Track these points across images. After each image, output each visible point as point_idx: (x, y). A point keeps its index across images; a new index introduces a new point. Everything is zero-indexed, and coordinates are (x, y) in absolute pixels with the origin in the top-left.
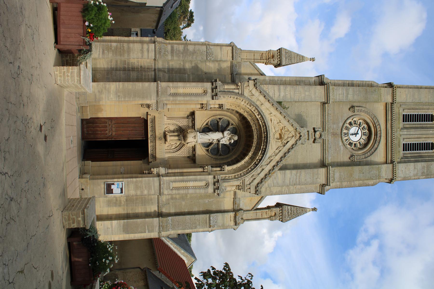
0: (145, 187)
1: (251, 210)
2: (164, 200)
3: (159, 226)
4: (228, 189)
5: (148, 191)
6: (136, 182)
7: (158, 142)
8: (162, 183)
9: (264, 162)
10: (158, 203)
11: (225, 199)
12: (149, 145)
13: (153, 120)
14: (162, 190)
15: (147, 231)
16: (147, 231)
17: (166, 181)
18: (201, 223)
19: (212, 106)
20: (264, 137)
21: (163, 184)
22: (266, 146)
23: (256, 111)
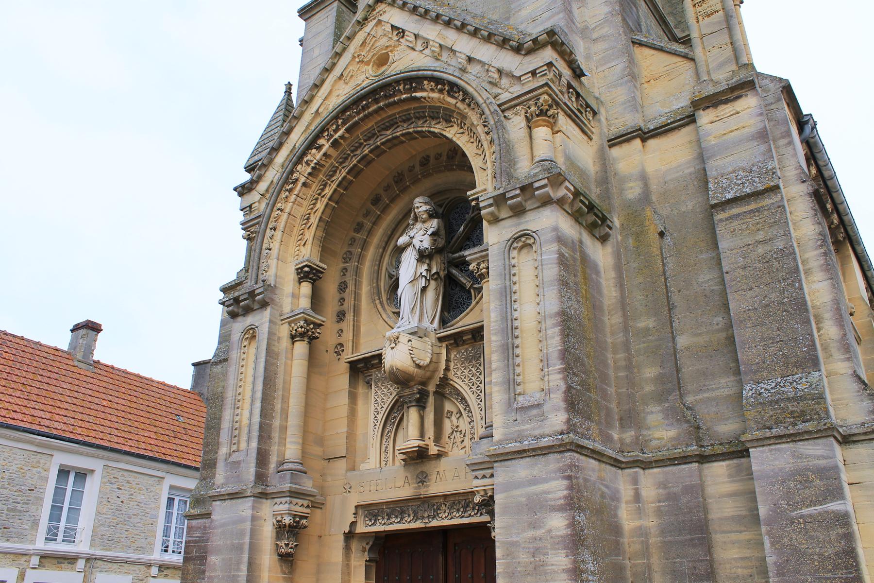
0: (534, 526)
1: (693, 60)
2: (672, 433)
3: (794, 438)
4: (542, 151)
5: (554, 509)
7: (436, 488)
8: (513, 446)
9: (448, 69)
10: (685, 459)
11: (650, 169)
12: (447, 522)
13: (371, 511)
14: (545, 442)
15: (834, 506)
16: (834, 506)
17: (506, 425)
19: (305, 303)
20: (377, 101)
21: (520, 439)
22: (397, 82)
23: (308, 157)
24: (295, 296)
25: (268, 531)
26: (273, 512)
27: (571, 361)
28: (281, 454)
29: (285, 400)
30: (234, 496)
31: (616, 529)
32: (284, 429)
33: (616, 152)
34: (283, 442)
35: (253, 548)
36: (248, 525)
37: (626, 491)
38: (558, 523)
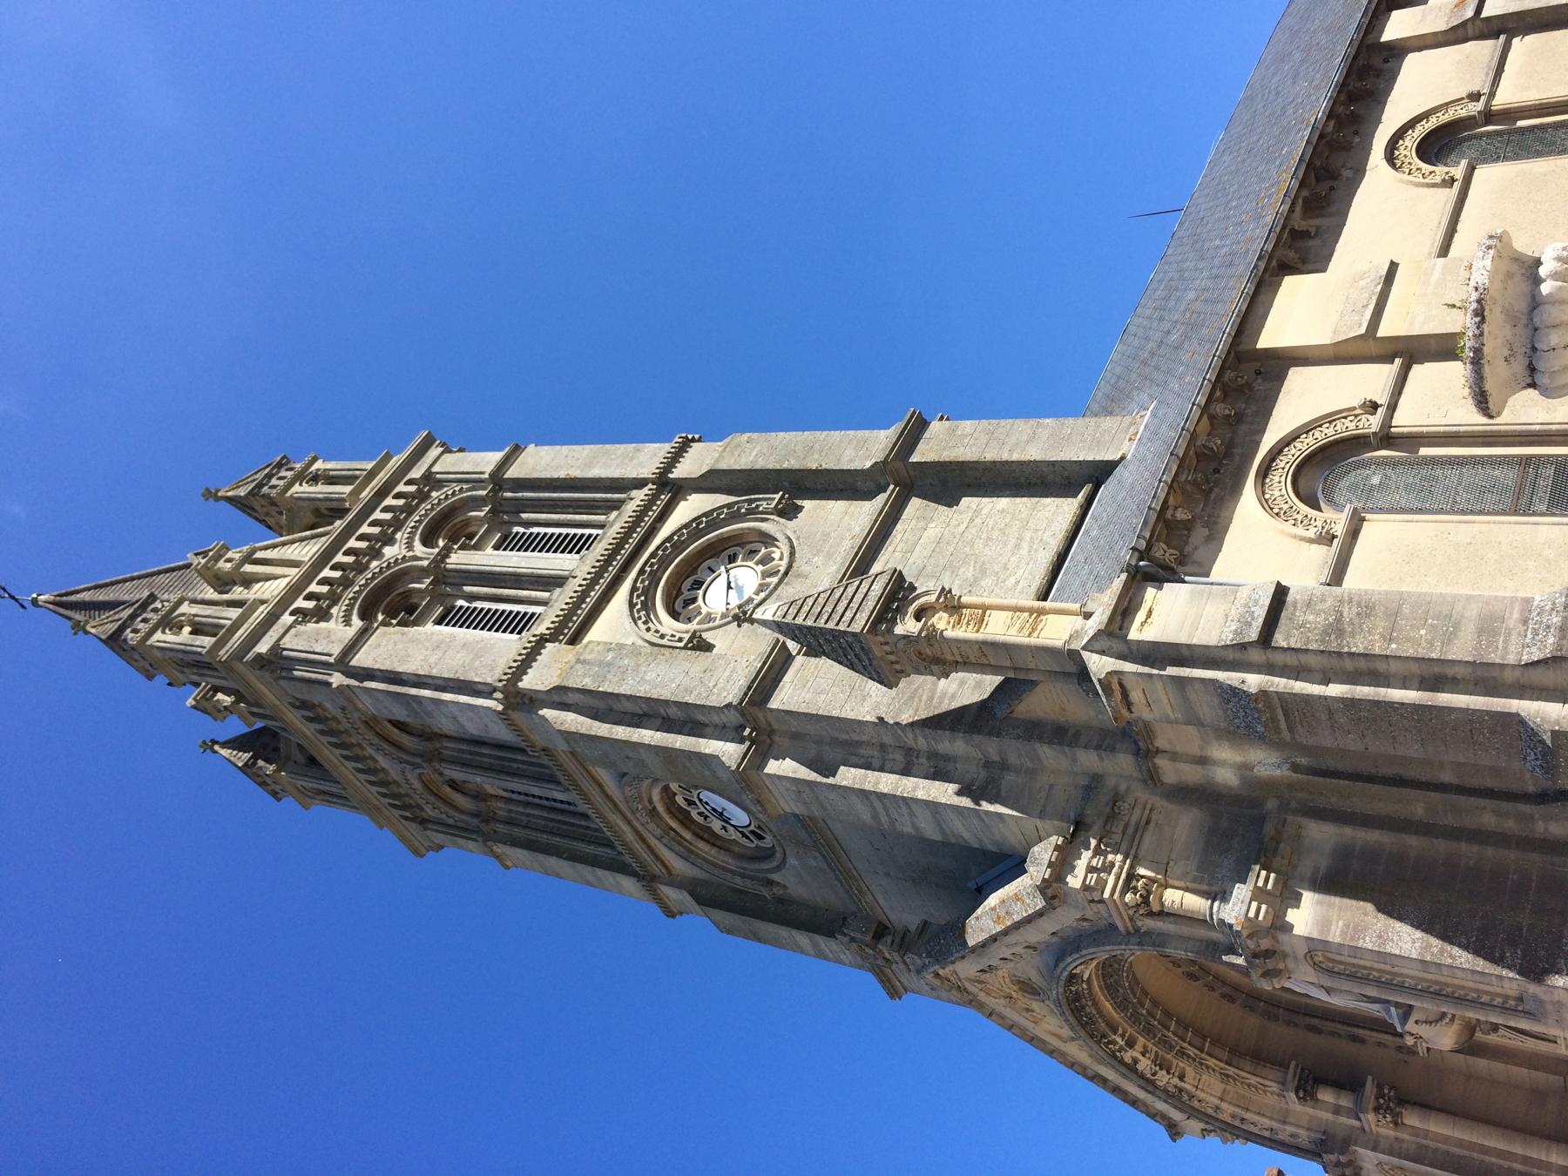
29: (1486, 1150)
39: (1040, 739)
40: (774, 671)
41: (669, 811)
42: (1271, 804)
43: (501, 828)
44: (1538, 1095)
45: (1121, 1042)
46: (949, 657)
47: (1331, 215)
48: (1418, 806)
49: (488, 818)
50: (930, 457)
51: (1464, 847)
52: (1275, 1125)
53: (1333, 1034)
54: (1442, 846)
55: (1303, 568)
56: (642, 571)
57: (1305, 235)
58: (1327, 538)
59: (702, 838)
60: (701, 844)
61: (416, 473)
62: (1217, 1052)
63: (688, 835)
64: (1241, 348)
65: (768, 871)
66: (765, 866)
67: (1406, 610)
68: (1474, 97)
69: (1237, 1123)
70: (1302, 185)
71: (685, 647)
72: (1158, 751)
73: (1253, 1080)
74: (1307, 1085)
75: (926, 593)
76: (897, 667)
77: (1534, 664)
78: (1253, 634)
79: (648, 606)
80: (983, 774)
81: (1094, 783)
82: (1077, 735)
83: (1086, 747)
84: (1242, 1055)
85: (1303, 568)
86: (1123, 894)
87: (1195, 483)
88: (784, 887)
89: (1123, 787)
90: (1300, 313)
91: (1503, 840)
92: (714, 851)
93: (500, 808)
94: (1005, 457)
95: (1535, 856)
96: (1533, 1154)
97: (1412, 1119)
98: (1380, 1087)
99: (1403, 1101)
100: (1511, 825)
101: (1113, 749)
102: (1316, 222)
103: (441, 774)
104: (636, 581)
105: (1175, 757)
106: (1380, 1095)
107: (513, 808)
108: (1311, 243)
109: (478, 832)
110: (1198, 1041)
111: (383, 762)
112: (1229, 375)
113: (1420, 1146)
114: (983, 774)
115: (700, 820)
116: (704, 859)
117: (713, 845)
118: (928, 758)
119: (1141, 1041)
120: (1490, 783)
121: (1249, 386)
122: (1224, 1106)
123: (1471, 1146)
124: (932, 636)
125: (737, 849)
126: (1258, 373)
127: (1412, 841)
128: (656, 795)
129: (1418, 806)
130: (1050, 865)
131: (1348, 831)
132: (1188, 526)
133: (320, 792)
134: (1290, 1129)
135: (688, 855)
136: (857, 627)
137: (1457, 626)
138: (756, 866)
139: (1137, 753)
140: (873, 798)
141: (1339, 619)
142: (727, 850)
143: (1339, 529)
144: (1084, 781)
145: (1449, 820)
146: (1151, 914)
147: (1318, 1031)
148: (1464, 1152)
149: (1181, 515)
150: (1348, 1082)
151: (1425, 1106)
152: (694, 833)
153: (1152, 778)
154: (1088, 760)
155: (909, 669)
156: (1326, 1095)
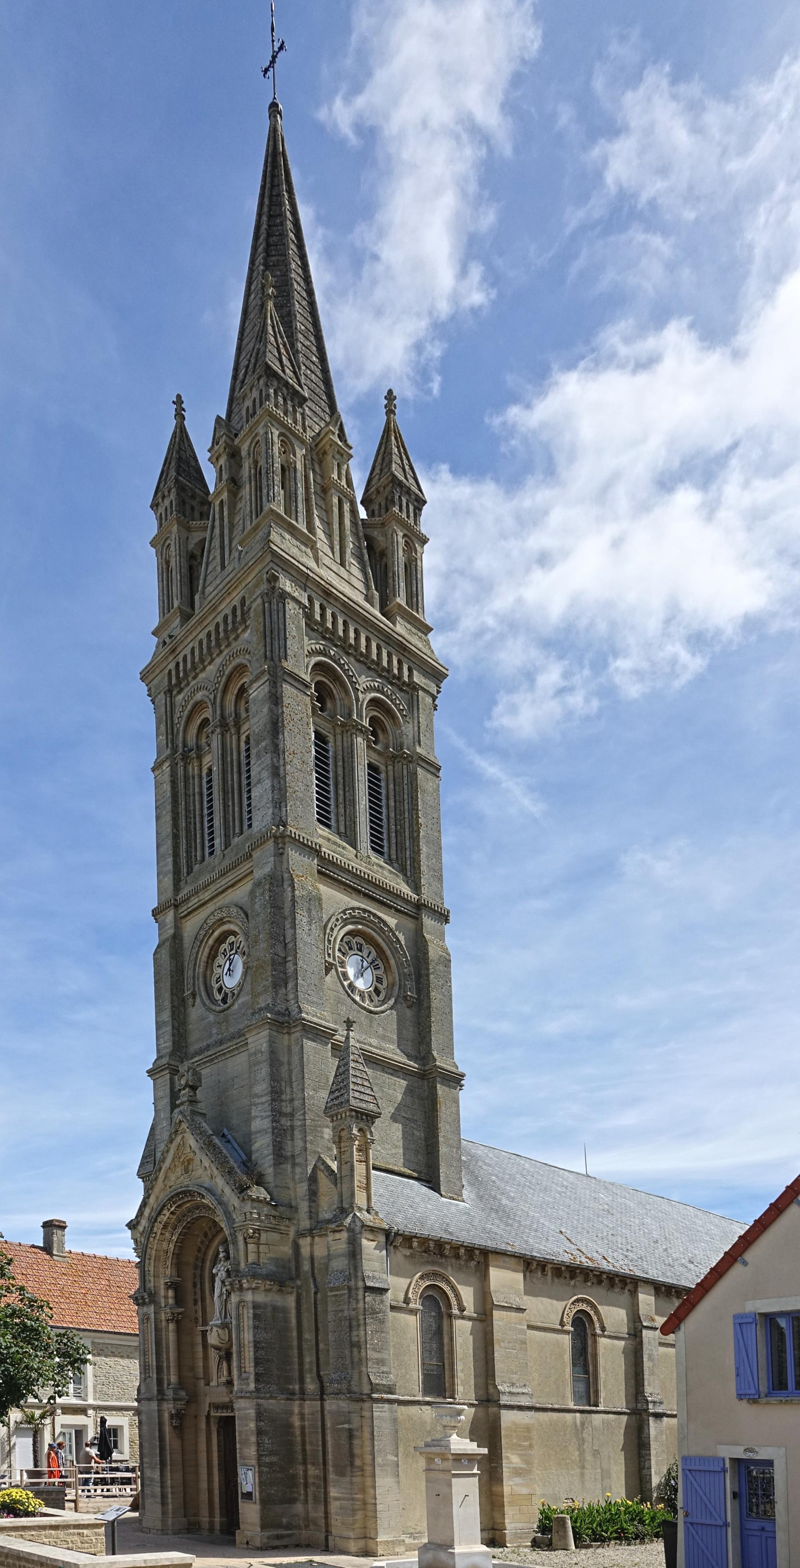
5: (251, 1420)
6: (240, 1443)
18: (340, 1308)
24: (166, 1297)
25: (166, 1416)
26: (169, 1407)
27: (257, 1362)
28: (169, 1380)
29: (168, 1353)
30: (149, 1399)
31: (290, 1426)
32: (168, 1367)
33: (305, 1242)
34: (169, 1374)
35: (161, 1424)
36: (156, 1414)
37: (296, 1410)
38: (252, 1425)
39: (310, 1185)
40: (320, 1034)
41: (224, 932)
42: (299, 1283)
43: (180, 771)
44: (193, 1369)
45: (172, 1209)
46: (342, 1145)
47: (552, 1280)
48: (308, 1336)
49: (185, 758)
50: (440, 1092)
51: (296, 1351)
52: (152, 1273)
53: (195, 1293)
54: (295, 1343)
55: (394, 1296)
56: (365, 911)
57: (543, 1270)
58: (407, 1301)
59: (211, 950)
60: (207, 950)
61: (418, 678)
62: (177, 1248)
63: (211, 942)
64: (490, 1256)
65: (201, 996)
66: (203, 994)
67: (383, 1335)
68: (603, 1329)
69: (147, 1257)
70: (567, 1267)
71: (326, 961)
72: (313, 1237)
73: (169, 1263)
74: (173, 1285)
75: (371, 1133)
76: (335, 1118)
77: (369, 1376)
78: (370, 1284)
79: (346, 922)
80: (289, 1154)
81: (293, 1208)
82: (314, 1201)
83: (310, 1206)
84: (178, 1258)
85: (394, 1296)
86: (252, 1228)
87: (429, 1247)
88: (193, 1006)
89: (295, 1222)
90: (504, 1280)
91: (301, 1364)
92: (204, 958)
93: (193, 769)
94: (441, 1134)
95: (297, 1374)
96: (172, 1369)
97: (172, 1326)
98: (181, 1313)
99: (178, 1322)
100: (307, 1366)
101: (311, 1218)
102: (550, 1274)
103: (212, 732)
104: (359, 909)
105: (312, 1245)
106: (179, 1314)
107: (196, 780)
108: (540, 1273)
109: (174, 750)
110: (179, 1240)
111: (211, 669)
112: (477, 1252)
113: (162, 1329)
114: (289, 1154)
115: (221, 950)
116: (197, 953)
117: (208, 958)
118: (291, 1126)
119: (174, 1217)
120: (322, 1361)
121: (473, 1259)
122: (154, 1252)
123: (168, 1348)
124: (352, 1139)
125: (208, 973)
126: (479, 1262)
127: (295, 1334)
128: (232, 927)
129: (308, 1336)
130: (258, 1197)
131: (294, 1311)
132: (411, 1247)
133: (168, 563)
134: (152, 1279)
135: (198, 940)
136: (353, 1102)
137: (379, 1352)
138: (202, 989)
139: (311, 1230)
140: (158, 803)
141: (377, 1313)
142: (207, 967)
143: (412, 1305)
144: (293, 1204)
145: (305, 1346)
146: (245, 1239)
147: (195, 1285)
148: (164, 1346)
149: (415, 1244)
150: (179, 1300)
151: (179, 1331)
152: (213, 946)
153: (300, 1235)
154: (304, 1206)
155: (335, 1123)
156: (171, 1293)
